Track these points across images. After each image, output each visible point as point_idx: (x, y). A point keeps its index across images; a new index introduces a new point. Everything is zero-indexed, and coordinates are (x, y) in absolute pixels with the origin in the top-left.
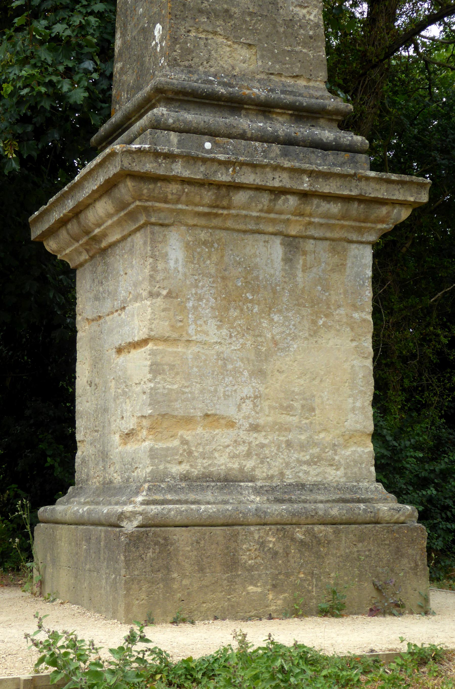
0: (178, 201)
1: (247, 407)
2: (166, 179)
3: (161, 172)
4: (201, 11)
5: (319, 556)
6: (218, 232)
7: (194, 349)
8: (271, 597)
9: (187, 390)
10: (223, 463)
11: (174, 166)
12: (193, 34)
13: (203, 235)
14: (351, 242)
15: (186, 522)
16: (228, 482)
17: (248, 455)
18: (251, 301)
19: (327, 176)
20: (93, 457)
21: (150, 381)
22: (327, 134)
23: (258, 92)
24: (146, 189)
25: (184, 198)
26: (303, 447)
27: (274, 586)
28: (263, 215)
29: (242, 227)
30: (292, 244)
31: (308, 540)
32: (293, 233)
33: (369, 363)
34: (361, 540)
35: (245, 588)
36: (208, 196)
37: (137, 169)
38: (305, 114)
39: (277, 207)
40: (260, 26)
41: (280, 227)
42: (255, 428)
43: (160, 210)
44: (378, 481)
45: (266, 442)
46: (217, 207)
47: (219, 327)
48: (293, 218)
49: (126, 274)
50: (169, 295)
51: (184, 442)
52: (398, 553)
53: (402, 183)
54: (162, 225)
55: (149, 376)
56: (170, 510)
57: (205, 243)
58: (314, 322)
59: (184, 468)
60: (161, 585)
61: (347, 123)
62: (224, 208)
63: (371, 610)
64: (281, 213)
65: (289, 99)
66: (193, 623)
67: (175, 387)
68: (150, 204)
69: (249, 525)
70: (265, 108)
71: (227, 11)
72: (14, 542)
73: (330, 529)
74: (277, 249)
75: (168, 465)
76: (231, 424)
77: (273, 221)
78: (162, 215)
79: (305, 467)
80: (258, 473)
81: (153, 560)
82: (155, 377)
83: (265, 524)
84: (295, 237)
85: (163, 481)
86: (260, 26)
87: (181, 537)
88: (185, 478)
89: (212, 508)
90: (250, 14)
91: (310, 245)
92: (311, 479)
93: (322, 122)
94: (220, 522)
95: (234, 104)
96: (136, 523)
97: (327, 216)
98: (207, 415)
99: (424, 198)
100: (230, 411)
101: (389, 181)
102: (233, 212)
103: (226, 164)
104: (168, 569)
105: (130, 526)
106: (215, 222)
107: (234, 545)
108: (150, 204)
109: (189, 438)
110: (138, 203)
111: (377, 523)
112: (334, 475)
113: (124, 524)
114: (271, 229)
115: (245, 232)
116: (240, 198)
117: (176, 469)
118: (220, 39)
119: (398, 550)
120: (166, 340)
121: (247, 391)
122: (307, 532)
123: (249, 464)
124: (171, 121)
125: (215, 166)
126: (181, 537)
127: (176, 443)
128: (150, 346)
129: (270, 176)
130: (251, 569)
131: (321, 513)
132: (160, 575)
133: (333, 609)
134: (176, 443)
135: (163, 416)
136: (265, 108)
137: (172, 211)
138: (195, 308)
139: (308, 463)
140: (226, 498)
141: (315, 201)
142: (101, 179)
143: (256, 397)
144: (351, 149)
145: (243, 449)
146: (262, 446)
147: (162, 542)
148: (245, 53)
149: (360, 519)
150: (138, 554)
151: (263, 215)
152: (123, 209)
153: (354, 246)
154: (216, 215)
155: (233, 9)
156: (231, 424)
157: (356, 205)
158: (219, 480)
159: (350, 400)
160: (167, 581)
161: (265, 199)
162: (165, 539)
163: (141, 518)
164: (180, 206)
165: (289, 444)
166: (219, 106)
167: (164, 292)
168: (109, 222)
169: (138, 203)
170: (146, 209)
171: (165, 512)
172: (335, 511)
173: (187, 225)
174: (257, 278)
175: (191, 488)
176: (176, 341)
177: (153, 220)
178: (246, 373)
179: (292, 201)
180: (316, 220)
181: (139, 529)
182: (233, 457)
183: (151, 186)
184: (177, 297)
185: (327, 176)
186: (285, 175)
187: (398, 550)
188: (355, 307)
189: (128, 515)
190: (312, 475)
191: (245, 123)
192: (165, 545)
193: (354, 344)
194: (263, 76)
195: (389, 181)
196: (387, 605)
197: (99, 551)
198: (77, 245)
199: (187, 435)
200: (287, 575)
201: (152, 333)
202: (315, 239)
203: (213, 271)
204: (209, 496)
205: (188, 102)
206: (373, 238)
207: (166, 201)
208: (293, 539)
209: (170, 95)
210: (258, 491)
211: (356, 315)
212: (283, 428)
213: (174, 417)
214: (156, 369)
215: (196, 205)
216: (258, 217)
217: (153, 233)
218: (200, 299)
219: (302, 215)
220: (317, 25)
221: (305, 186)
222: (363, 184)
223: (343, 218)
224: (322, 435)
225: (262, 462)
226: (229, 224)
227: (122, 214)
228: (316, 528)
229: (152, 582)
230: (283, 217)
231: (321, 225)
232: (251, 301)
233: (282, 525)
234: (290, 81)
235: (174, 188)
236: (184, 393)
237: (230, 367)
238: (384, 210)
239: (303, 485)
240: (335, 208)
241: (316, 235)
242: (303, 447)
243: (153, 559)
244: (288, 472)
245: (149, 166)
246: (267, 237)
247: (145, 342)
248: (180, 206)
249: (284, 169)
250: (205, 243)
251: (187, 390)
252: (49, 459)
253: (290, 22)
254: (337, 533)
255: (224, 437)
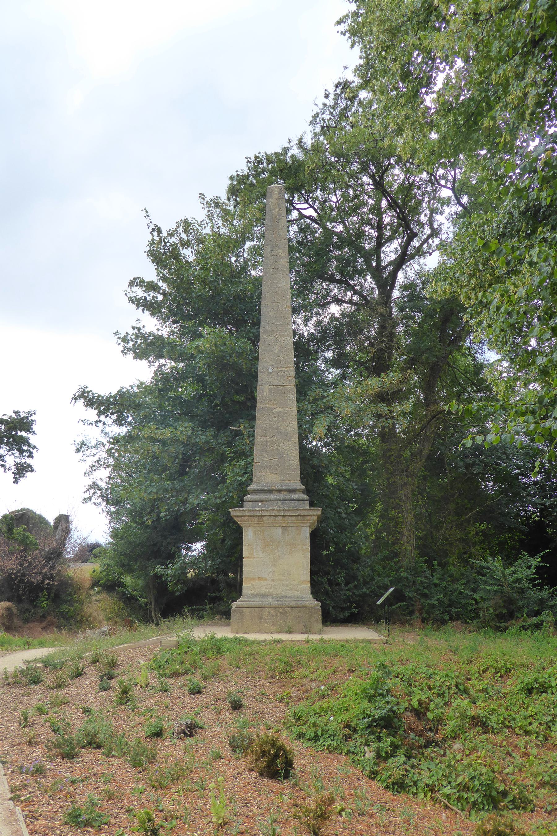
1: (271, 575)
5: (286, 616)
7: (255, 559)
10: (263, 590)
13: (258, 529)
16: (264, 595)
17: (271, 588)
19: (289, 510)
22: (295, 496)
23: (277, 487)
26: (287, 585)
30: (284, 528)
33: (309, 561)
34: (299, 612)
36: (256, 519)
42: (273, 580)
51: (252, 585)
52: (311, 616)
59: (253, 592)
70: (279, 491)
74: (280, 530)
76: (266, 580)
87: (245, 610)
88: (253, 594)
89: (255, 603)
92: (290, 595)
95: (270, 491)
99: (319, 513)
100: (266, 576)
103: (259, 511)
112: (297, 593)
116: (265, 518)
119: (311, 615)
121: (270, 570)
126: (245, 610)
133: (290, 632)
136: (279, 491)
144: (303, 500)
145: (269, 586)
148: (276, 476)
156: (266, 580)
161: (272, 518)
165: (283, 585)
172: (291, 604)
175: (253, 597)
176: (251, 557)
182: (266, 589)
185: (289, 510)
187: (311, 615)
188: (304, 545)
190: (290, 593)
191: (271, 496)
196: (307, 631)
199: (254, 583)
204: (258, 600)
210: (272, 598)
212: (281, 580)
233: (275, 608)
238: (309, 517)
240: (293, 518)
242: (287, 585)
255: (264, 583)
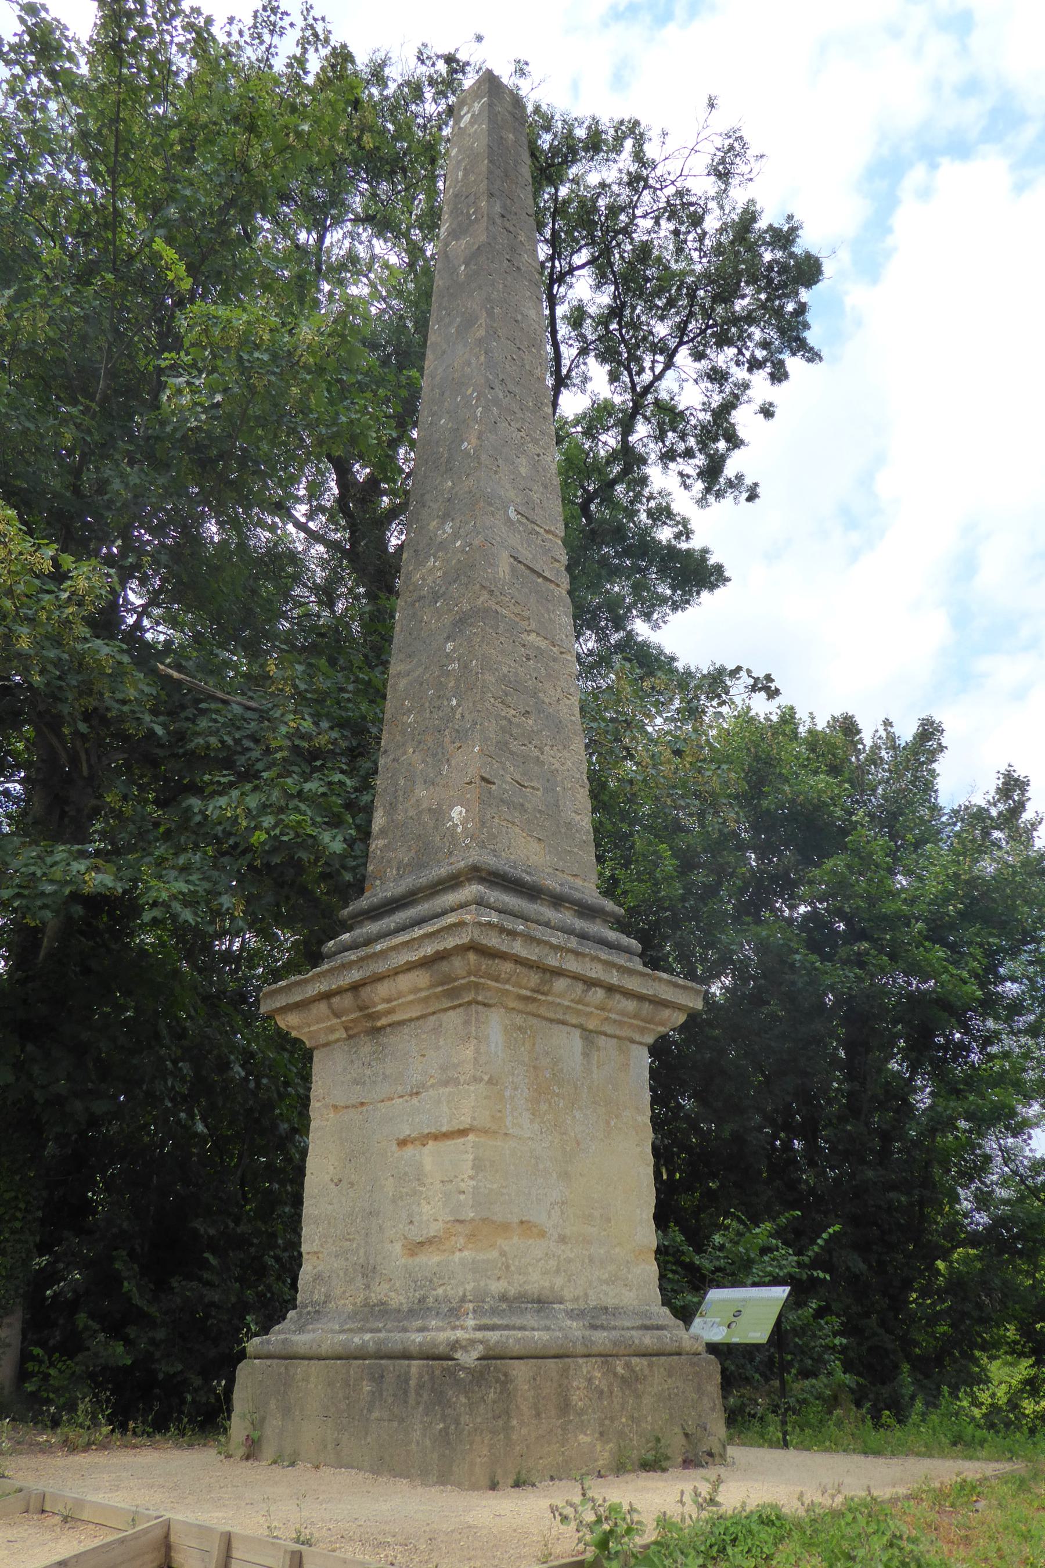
0: (507, 981)
2: (503, 956)
3: (504, 948)
4: (502, 801)
6: (530, 1018)
8: (599, 1448)
9: (504, 1191)
10: (536, 1282)
11: (514, 944)
12: (496, 820)
13: (519, 1020)
14: (632, 1041)
15: (523, 1352)
16: (542, 1303)
18: (558, 1095)
20: (341, 1273)
21: (471, 1178)
24: (485, 964)
25: (514, 979)
27: (601, 1434)
28: (574, 1005)
29: (551, 1015)
30: (589, 1035)
31: (627, 1375)
32: (591, 1027)
35: (576, 1437)
37: (484, 942)
38: (586, 911)
39: (587, 999)
40: (547, 824)
41: (582, 1020)
42: (563, 1239)
43: (489, 989)
44: (663, 1304)
45: (572, 1256)
46: (537, 991)
47: (532, 1121)
48: (596, 1011)
49: (423, 1056)
50: (490, 1082)
51: (503, 1254)
52: (699, 1390)
53: (684, 988)
54: (485, 1005)
55: (471, 1172)
56: (508, 1337)
57: (520, 1028)
58: (608, 1123)
60: (502, 1436)
61: (622, 926)
62: (543, 994)
63: (684, 1461)
64: (587, 1005)
65: (577, 895)
66: (533, 1485)
67: (495, 1186)
68: (482, 980)
69: (576, 1356)
71: (522, 805)
72: (219, 1384)
73: (644, 1361)
75: (489, 1282)
77: (578, 1013)
78: (489, 994)
79: (605, 1287)
80: (567, 1294)
81: (445, 1402)
82: (477, 1173)
83: (589, 1356)
84: (591, 1031)
85: (483, 1301)
86: (547, 824)
88: (503, 1298)
90: (540, 811)
91: (602, 1041)
93: (598, 921)
94: (552, 1352)
95: (532, 892)
96: (475, 1355)
97: (623, 1013)
98: (522, 1222)
101: (676, 985)
102: (549, 998)
104: (507, 1413)
105: (468, 1358)
106: (532, 1007)
107: (566, 1382)
108: (482, 980)
109: (506, 1249)
110: (473, 978)
111: (679, 1354)
113: (457, 1355)
114: (574, 1021)
115: (551, 1021)
116: (560, 984)
117: (496, 1287)
118: (517, 830)
120: (486, 1132)
122: (627, 1365)
123: (559, 1281)
124: (492, 900)
125: (547, 950)
126: (520, 1371)
127: (495, 1254)
128: (471, 1137)
129: (588, 966)
130: (581, 1413)
131: (637, 1342)
132: (501, 1423)
134: (495, 1254)
135: (484, 1220)
137: (498, 990)
138: (512, 1098)
139: (606, 1282)
140: (548, 1323)
141: (618, 996)
142: (429, 949)
143: (563, 1203)
145: (553, 1263)
146: (569, 1261)
147: (503, 1378)
148: (535, 846)
149: (668, 1349)
150: (480, 1395)
151: (574, 1005)
152: (442, 984)
153: (635, 1046)
154: (535, 1000)
155: (527, 805)
156: (542, 1234)
157: (647, 1005)
158: (533, 1302)
159: (638, 1211)
160: (507, 1429)
161: (580, 987)
162: (506, 1375)
163: (481, 1348)
164: (507, 987)
166: (522, 892)
167: (486, 1078)
168: (411, 997)
169: (473, 978)
170: (477, 985)
171: (504, 1339)
173: (506, 1008)
174: (562, 1070)
177: (480, 998)
178: (554, 1175)
179: (600, 994)
180: (613, 1016)
181: (485, 1362)
183: (490, 962)
184: (496, 1084)
186: (600, 967)
189: (464, 1343)
192: (505, 1382)
193: (639, 1149)
194: (550, 870)
195: (676, 985)
197: (406, 1392)
198: (335, 1021)
200: (612, 1419)
201: (475, 1123)
202: (606, 1035)
203: (526, 1060)
205: (497, 884)
206: (650, 1040)
207: (497, 981)
208: (615, 1374)
209: (483, 875)
210: (570, 1314)
211: (639, 1119)
213: (494, 1222)
214: (478, 1165)
215: (521, 987)
216: (568, 1007)
217: (477, 1012)
218: (516, 1089)
219: (603, 1009)
220: (588, 831)
221: (615, 981)
222: (656, 984)
223: (635, 1016)
224: (617, 1250)
225: (569, 1281)
226: (543, 1011)
227: (440, 989)
228: (635, 1360)
229: (494, 1432)
230: (588, 1009)
231: (615, 1021)
232: (558, 1095)
234: (570, 878)
235: (508, 967)
236: (503, 1194)
237: (541, 1166)
238: (666, 1013)
239: (606, 1308)
240: (631, 1005)
241: (609, 1032)
243: (494, 1402)
244: (591, 1292)
245: (493, 941)
246: (569, 1029)
247: (463, 1133)
248: (507, 987)
249: (599, 960)
250: (520, 1028)
251: (504, 1191)
252: (126, 1284)
253: (569, 825)
254: (650, 1365)
